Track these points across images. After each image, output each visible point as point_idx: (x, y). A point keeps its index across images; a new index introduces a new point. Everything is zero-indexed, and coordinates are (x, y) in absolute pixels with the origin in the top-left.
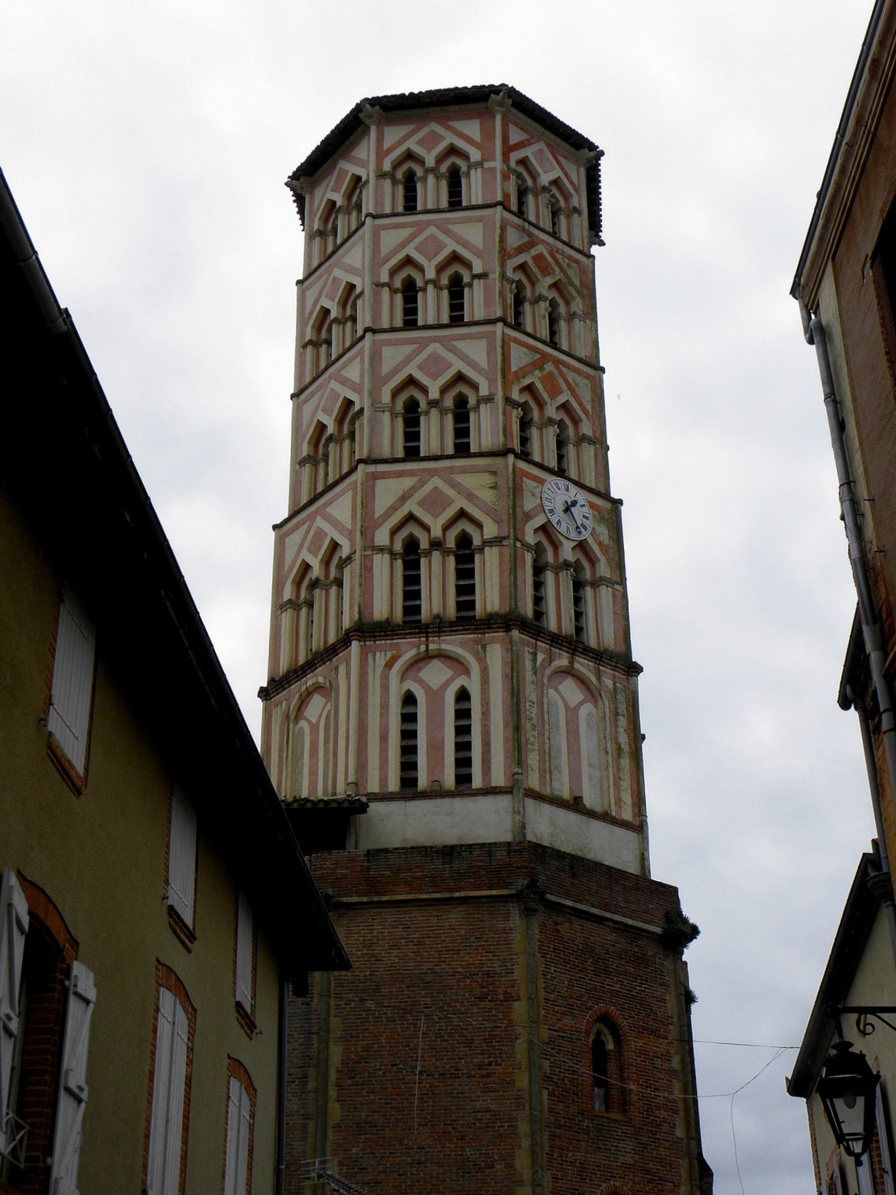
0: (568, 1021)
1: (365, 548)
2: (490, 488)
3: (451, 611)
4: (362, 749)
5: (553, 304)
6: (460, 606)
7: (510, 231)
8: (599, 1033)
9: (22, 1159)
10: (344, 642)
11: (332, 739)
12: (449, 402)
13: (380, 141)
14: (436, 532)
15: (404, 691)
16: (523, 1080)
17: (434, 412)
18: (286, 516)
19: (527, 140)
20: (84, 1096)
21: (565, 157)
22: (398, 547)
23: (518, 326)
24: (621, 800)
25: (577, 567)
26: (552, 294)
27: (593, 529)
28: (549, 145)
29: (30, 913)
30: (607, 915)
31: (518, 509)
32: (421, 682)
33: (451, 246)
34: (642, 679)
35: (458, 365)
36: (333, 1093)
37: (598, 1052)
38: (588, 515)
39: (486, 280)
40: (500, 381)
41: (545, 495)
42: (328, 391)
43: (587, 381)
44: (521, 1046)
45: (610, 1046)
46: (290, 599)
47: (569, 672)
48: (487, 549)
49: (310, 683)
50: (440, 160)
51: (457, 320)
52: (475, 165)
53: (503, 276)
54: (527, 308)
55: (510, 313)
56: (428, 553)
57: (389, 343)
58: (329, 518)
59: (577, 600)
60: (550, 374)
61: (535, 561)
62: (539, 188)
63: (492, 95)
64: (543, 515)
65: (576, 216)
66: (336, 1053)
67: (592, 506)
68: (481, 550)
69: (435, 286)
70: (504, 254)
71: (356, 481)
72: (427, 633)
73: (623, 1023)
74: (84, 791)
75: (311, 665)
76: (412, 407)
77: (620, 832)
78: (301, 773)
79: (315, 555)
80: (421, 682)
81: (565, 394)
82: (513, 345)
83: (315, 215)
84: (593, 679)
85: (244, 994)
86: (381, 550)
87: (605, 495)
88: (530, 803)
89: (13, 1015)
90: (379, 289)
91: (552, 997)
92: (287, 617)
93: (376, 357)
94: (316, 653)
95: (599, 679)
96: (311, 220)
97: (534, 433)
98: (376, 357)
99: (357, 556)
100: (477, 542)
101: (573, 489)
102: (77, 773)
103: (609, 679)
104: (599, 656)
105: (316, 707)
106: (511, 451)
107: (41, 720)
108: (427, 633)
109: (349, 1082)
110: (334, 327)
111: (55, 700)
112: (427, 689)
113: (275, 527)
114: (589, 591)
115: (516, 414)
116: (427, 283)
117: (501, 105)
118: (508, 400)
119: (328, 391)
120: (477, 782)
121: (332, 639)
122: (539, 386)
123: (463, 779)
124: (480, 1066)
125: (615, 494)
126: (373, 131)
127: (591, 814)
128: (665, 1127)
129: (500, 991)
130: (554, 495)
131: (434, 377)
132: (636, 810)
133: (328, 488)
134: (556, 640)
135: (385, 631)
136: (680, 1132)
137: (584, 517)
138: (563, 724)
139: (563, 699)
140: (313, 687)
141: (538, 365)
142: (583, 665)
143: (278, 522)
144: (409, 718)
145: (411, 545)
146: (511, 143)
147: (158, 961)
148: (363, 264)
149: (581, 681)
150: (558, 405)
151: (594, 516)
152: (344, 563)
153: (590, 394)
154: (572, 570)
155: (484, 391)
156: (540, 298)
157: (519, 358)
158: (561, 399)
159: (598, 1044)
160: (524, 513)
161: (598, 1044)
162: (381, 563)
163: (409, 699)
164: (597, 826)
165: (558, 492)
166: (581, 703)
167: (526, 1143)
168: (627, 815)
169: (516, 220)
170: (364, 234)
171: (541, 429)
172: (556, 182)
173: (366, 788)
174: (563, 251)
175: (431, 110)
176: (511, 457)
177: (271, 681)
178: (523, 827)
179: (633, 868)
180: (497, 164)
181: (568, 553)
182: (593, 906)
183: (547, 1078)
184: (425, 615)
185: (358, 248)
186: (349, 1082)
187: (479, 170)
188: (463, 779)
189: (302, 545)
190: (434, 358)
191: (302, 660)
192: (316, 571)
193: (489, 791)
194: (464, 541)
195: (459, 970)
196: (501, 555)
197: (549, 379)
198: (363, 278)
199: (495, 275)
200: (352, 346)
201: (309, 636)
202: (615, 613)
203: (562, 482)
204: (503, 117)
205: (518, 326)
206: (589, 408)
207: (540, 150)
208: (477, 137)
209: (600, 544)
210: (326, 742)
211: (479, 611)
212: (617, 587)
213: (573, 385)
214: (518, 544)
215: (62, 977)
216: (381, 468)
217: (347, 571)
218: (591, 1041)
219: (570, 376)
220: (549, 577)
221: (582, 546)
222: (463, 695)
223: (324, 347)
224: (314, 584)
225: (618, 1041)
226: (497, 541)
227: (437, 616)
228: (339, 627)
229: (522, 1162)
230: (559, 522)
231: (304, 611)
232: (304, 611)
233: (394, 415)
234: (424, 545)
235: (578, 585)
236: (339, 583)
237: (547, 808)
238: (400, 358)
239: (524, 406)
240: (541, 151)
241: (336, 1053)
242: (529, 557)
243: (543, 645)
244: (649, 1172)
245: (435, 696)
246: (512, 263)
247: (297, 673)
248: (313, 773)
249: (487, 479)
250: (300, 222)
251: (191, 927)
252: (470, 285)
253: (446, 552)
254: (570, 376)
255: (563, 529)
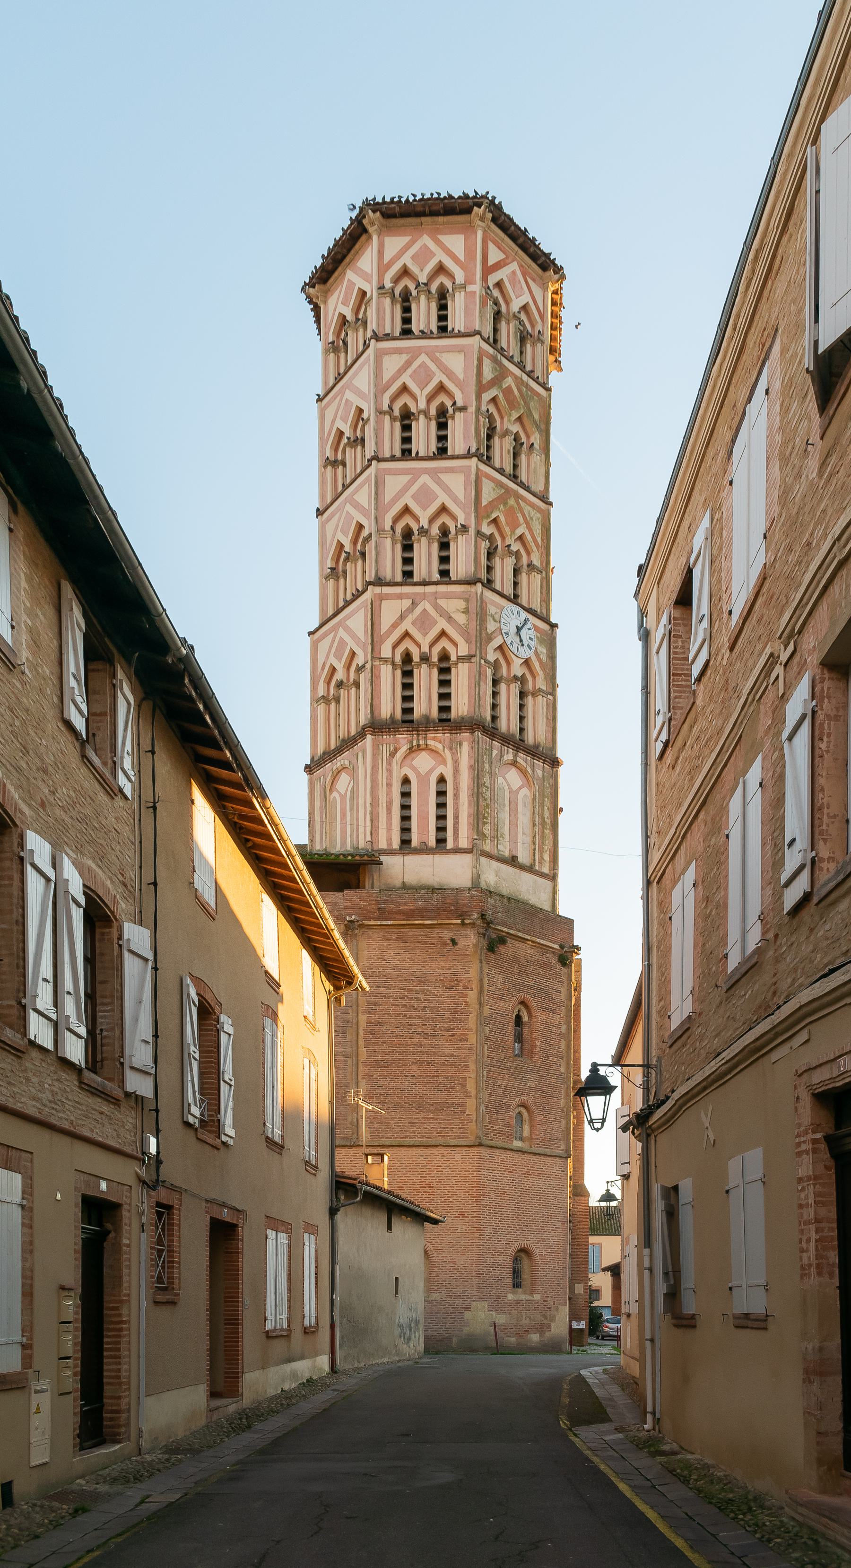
0: (501, 1004)
1: (373, 658)
2: (463, 612)
3: (435, 714)
4: (374, 820)
5: (516, 438)
6: (442, 709)
7: (486, 362)
8: (519, 1011)
9: (206, 1116)
10: (362, 734)
11: (355, 808)
12: (435, 531)
13: (381, 253)
14: (425, 649)
15: (402, 775)
16: (472, 1039)
17: (424, 540)
18: (317, 625)
19: (503, 260)
20: (232, 1083)
21: (534, 280)
22: (398, 659)
23: (488, 460)
24: (543, 859)
25: (522, 680)
26: (515, 428)
27: (536, 649)
28: (521, 266)
29: (198, 994)
30: (528, 937)
31: (483, 632)
32: (414, 769)
33: (439, 377)
34: (561, 770)
35: (443, 498)
36: (361, 1043)
37: (518, 1020)
38: (533, 637)
39: (465, 414)
40: (473, 515)
41: (502, 620)
42: (344, 514)
43: (538, 515)
44: (472, 1019)
45: (525, 1018)
46: (323, 696)
47: (514, 763)
48: (460, 664)
49: (339, 764)
50: (432, 277)
51: (442, 452)
52: (459, 288)
53: (478, 409)
54: (496, 440)
55: (483, 450)
56: (419, 665)
57: (390, 472)
58: (348, 630)
59: (522, 707)
60: (512, 507)
61: (494, 674)
62: (511, 315)
63: (475, 208)
64: (500, 636)
65: (539, 345)
66: (363, 1019)
67: (536, 628)
68: (456, 664)
69: (426, 416)
70: (481, 388)
71: (370, 475)
72: (418, 731)
73: (533, 1005)
74: (216, 917)
75: (339, 750)
76: (408, 534)
77: (541, 880)
78: (335, 830)
79: (340, 661)
80: (414, 769)
81: (522, 527)
82: (484, 480)
83: (329, 329)
84: (529, 770)
85: (308, 1010)
86: (385, 661)
87: (546, 620)
88: (483, 860)
89: (196, 1051)
90: (382, 416)
91: (492, 989)
92: (321, 708)
93: (379, 485)
94: (343, 740)
95: (533, 770)
96: (327, 334)
97: (497, 561)
98: (379, 485)
99: (368, 666)
100: (453, 658)
101: (524, 615)
102: (212, 908)
103: (540, 769)
104: (534, 752)
105: (344, 780)
106: (479, 580)
107: (191, 883)
108: (418, 731)
109: (371, 1036)
110: (348, 449)
111: (196, 869)
112: (418, 774)
113: (310, 634)
114: (530, 700)
115: (484, 545)
116: (419, 412)
117: (482, 219)
118: (479, 533)
119: (344, 514)
120: (450, 844)
121: (353, 732)
122: (502, 519)
123: (441, 841)
124: (448, 1030)
125: (554, 620)
126: (375, 238)
127: (522, 867)
128: (555, 1066)
129: (461, 984)
130: (509, 620)
131: (424, 508)
132: (552, 866)
133: (348, 603)
134: (506, 740)
135: (389, 729)
136: (563, 1070)
137: (531, 639)
138: (507, 803)
139: (509, 785)
140: (341, 768)
141: (502, 500)
142: (522, 758)
143: (312, 630)
144: (406, 795)
145: (407, 658)
146: (491, 261)
147: (262, 1003)
148: (372, 270)
149: (523, 772)
150: (516, 537)
151: (537, 637)
152: (360, 669)
153: (540, 527)
154: (519, 683)
155: (461, 520)
156: (506, 433)
157: (489, 493)
158: (519, 532)
159: (518, 1018)
160: (487, 634)
161: (518, 1018)
162: (386, 671)
163: (406, 781)
164: (527, 877)
165: (513, 617)
166: (520, 788)
167: (473, 1075)
168: (546, 870)
169: (491, 350)
170: (369, 356)
171: (503, 559)
172: (525, 308)
173: (378, 846)
174: (527, 384)
175: (424, 219)
176: (479, 585)
177: (312, 759)
178: (479, 877)
179: (547, 907)
180: (476, 288)
181: (518, 669)
182: (519, 931)
183: (487, 1038)
184: (416, 715)
185: (365, 370)
186: (371, 1036)
187: (463, 293)
188: (441, 841)
189: (330, 651)
190: (424, 488)
191: (333, 746)
192: (340, 675)
193: (457, 851)
194: (444, 657)
195: (437, 970)
196: (469, 669)
197: (510, 514)
198: (369, 404)
199: (472, 409)
200: (362, 472)
201: (337, 726)
202: (547, 718)
203: (515, 608)
204: (483, 233)
205: (488, 460)
206: (539, 540)
207: (513, 271)
208: (461, 255)
209: (540, 660)
210: (351, 809)
211: (453, 715)
212: (550, 697)
213: (528, 519)
214: (482, 661)
215: (215, 1023)
216: (386, 590)
217: (362, 676)
218: (514, 1016)
219: (527, 509)
220: (503, 687)
221: (527, 663)
222: (442, 780)
223: (341, 467)
224: (340, 685)
225: (530, 1015)
226: (468, 658)
227: (426, 716)
228: (358, 722)
229: (471, 1086)
230: (512, 643)
231: (333, 705)
232: (333, 705)
233: (394, 541)
234: (416, 658)
235: (522, 695)
236: (357, 685)
237: (495, 864)
238: (399, 487)
239: (491, 538)
240: (514, 272)
241: (363, 1019)
242: (489, 672)
243: (497, 743)
244: (543, 1092)
245: (423, 779)
246: (487, 396)
247: (329, 755)
248: (344, 832)
249: (462, 604)
250: (317, 332)
251: (277, 979)
252: (453, 417)
253: (431, 665)
254: (527, 509)
255: (514, 648)
